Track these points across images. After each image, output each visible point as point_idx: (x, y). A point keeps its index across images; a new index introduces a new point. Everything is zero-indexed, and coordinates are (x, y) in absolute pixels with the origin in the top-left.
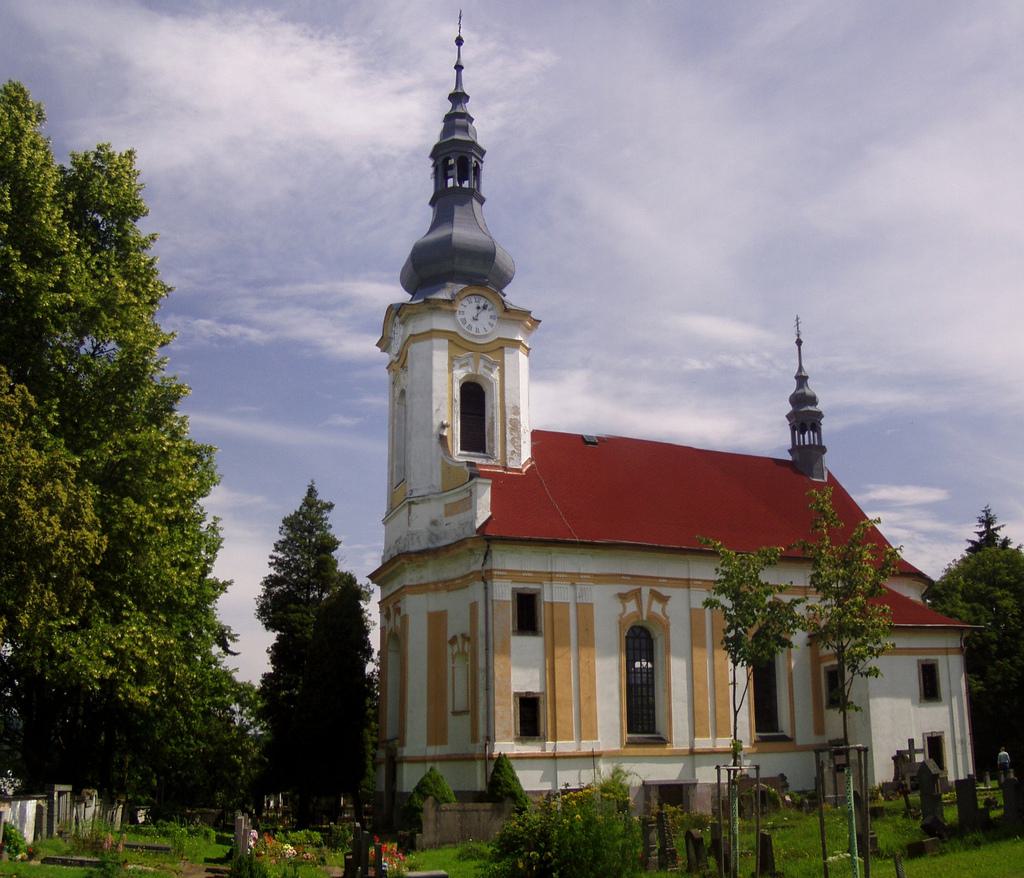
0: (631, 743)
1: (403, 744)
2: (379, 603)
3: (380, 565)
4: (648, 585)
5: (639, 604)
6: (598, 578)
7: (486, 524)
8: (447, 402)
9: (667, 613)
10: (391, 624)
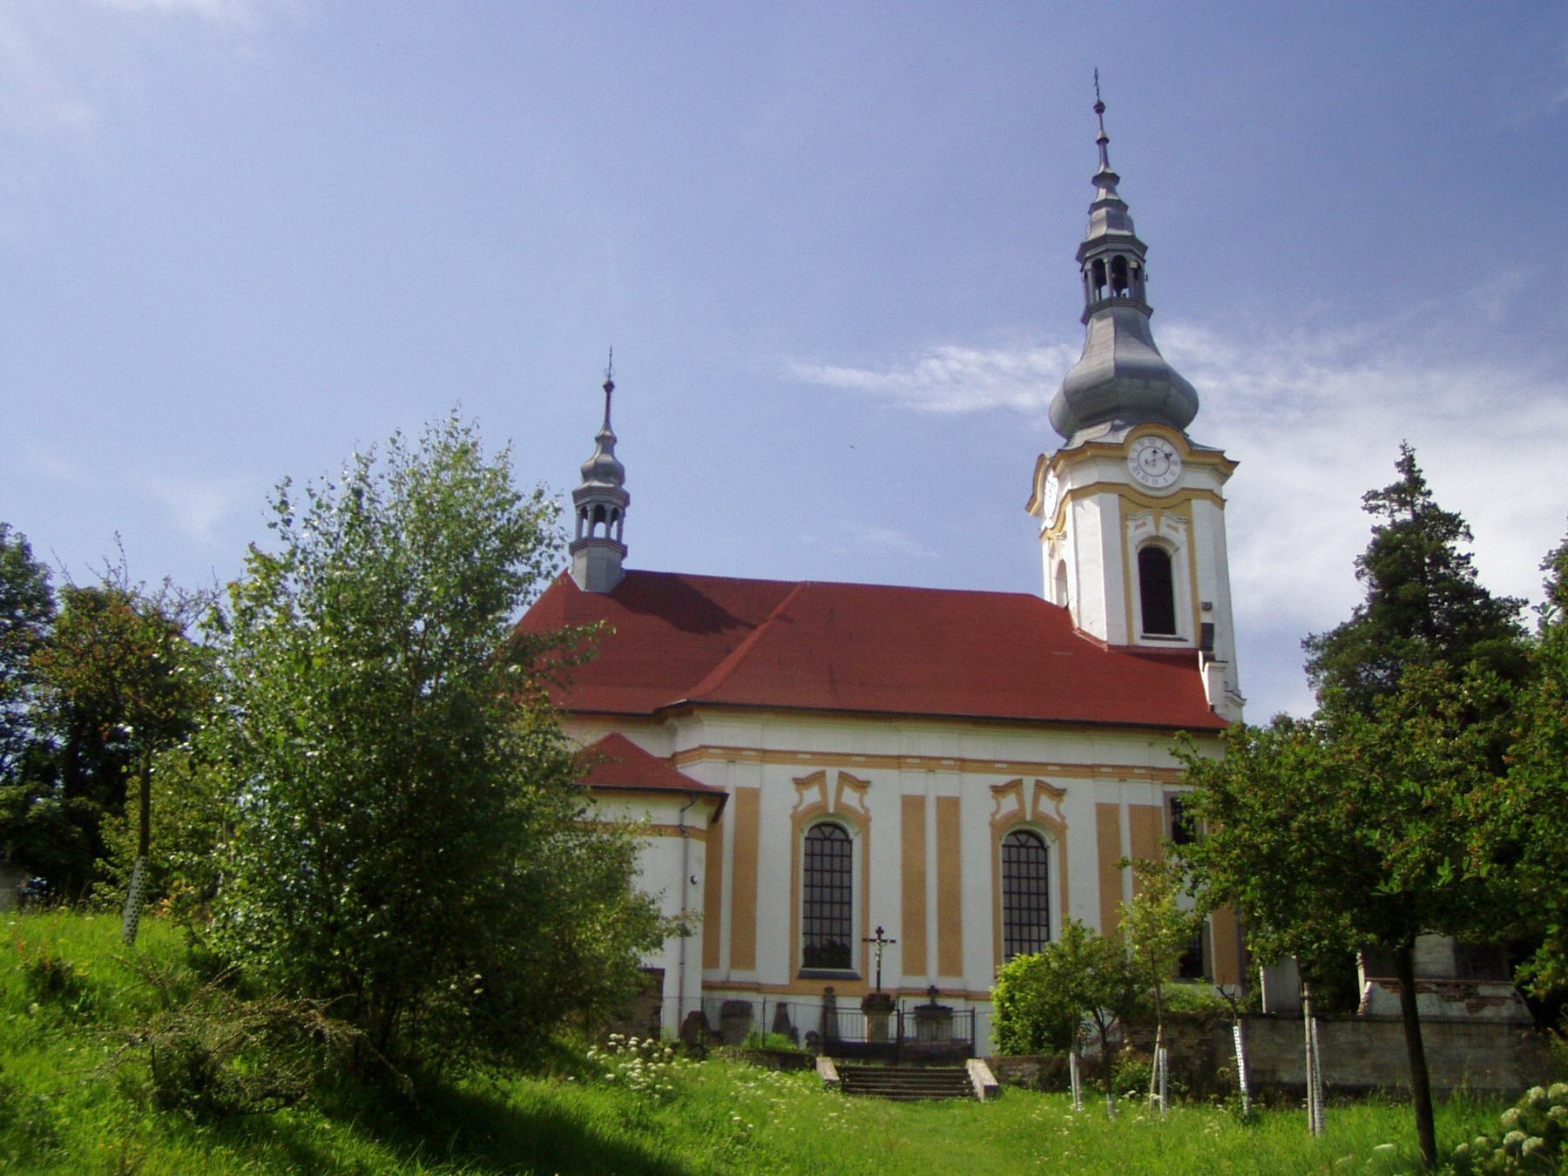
4: (1030, 774)
5: (824, 792)
6: (963, 764)
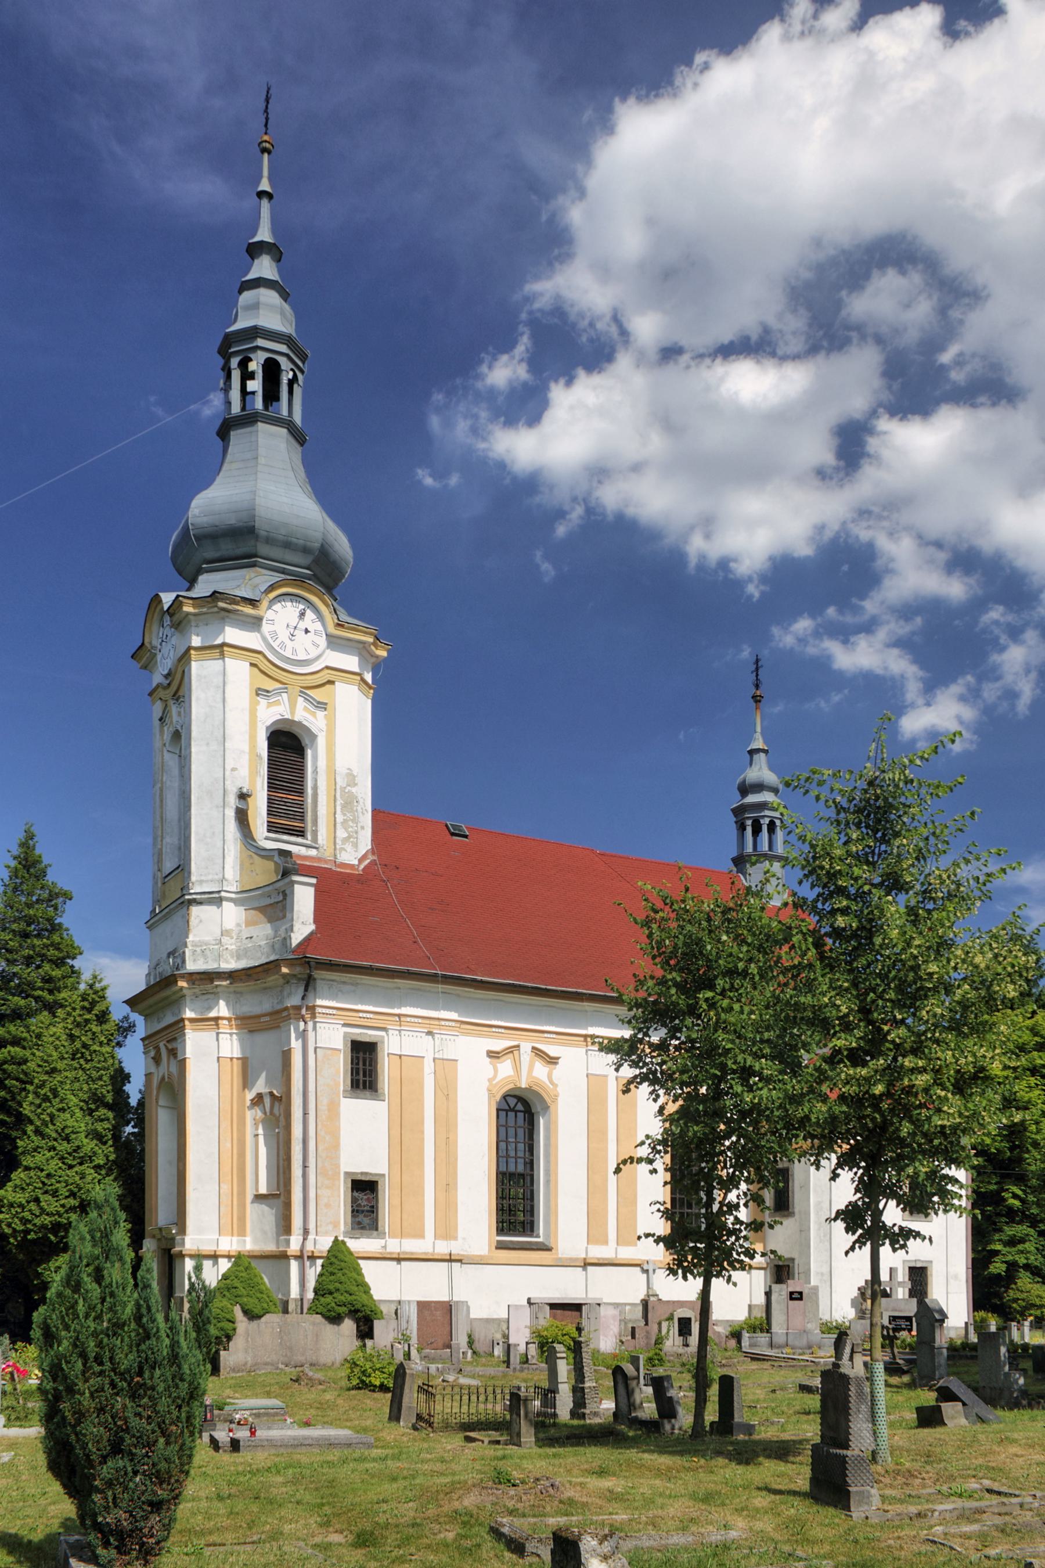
0: (501, 1246)
1: (183, 1230)
2: (142, 1040)
3: (143, 987)
7: (308, 940)
8: (245, 760)
9: (554, 1078)
10: (163, 1069)
